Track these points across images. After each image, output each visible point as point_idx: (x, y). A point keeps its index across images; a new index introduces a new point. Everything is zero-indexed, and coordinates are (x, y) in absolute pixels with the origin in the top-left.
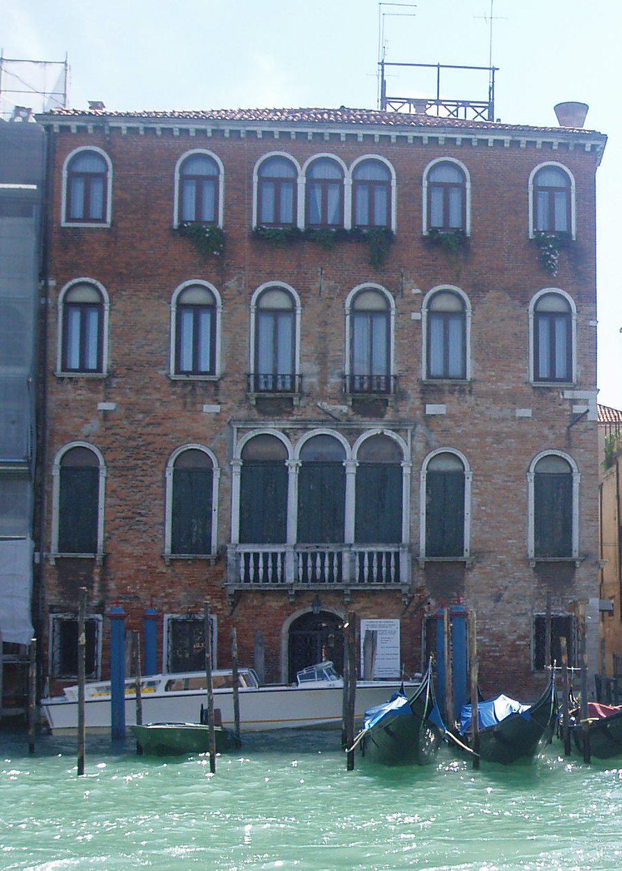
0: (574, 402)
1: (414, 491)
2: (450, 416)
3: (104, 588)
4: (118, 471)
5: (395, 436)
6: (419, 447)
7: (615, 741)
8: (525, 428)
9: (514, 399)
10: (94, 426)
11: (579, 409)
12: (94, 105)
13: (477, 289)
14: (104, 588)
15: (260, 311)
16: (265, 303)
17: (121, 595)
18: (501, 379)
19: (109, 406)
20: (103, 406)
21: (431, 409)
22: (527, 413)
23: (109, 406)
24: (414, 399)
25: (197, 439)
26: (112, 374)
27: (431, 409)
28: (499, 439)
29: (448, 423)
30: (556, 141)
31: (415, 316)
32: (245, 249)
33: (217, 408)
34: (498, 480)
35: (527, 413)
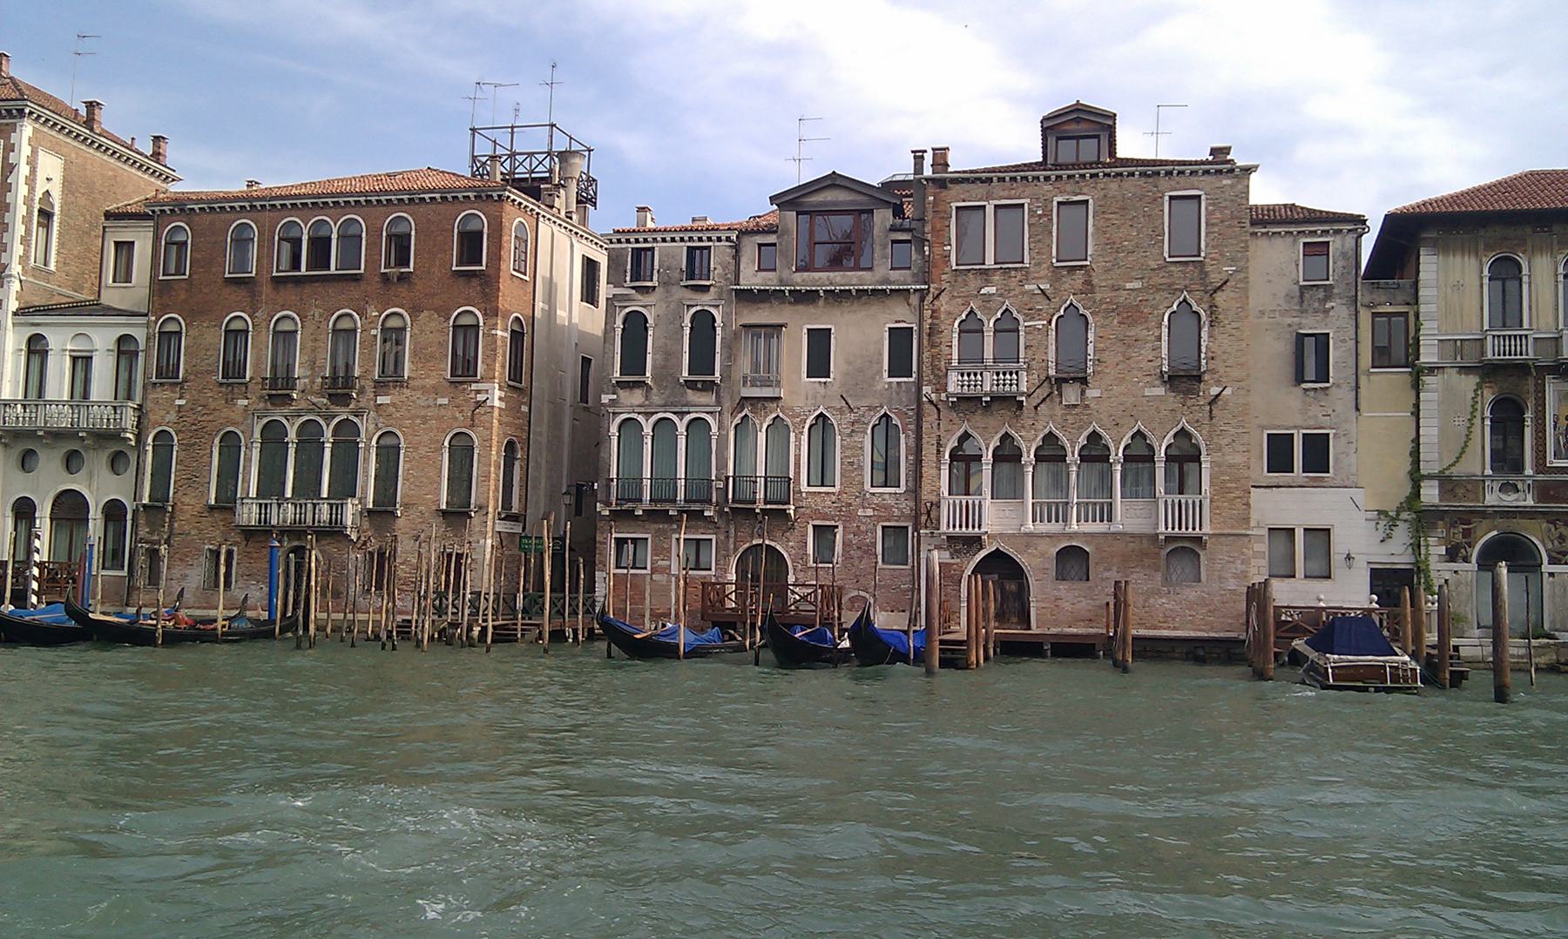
0: (478, 392)
1: (366, 460)
2: (394, 405)
3: (171, 526)
4: (186, 447)
5: (355, 420)
6: (371, 427)
7: (405, 631)
8: (443, 412)
9: (436, 391)
10: (172, 416)
11: (481, 397)
12: (250, 184)
13: (415, 311)
14: (171, 526)
15: (276, 333)
16: (280, 328)
17: (95, 526)
18: (428, 377)
19: (182, 402)
20: (178, 402)
21: (380, 400)
22: (445, 401)
23: (182, 402)
24: (370, 393)
25: (233, 424)
26: (185, 380)
27: (380, 400)
28: (425, 420)
29: (392, 409)
30: (471, 195)
31: (373, 332)
32: (266, 290)
33: (246, 402)
34: (423, 451)
35: (445, 401)
